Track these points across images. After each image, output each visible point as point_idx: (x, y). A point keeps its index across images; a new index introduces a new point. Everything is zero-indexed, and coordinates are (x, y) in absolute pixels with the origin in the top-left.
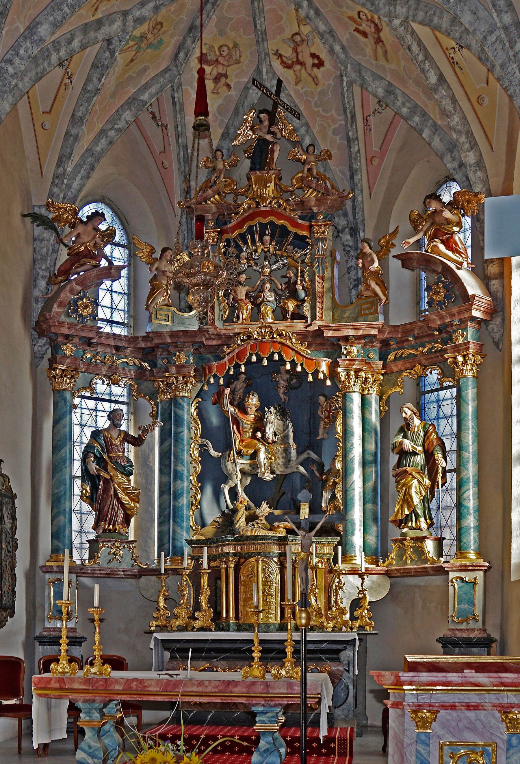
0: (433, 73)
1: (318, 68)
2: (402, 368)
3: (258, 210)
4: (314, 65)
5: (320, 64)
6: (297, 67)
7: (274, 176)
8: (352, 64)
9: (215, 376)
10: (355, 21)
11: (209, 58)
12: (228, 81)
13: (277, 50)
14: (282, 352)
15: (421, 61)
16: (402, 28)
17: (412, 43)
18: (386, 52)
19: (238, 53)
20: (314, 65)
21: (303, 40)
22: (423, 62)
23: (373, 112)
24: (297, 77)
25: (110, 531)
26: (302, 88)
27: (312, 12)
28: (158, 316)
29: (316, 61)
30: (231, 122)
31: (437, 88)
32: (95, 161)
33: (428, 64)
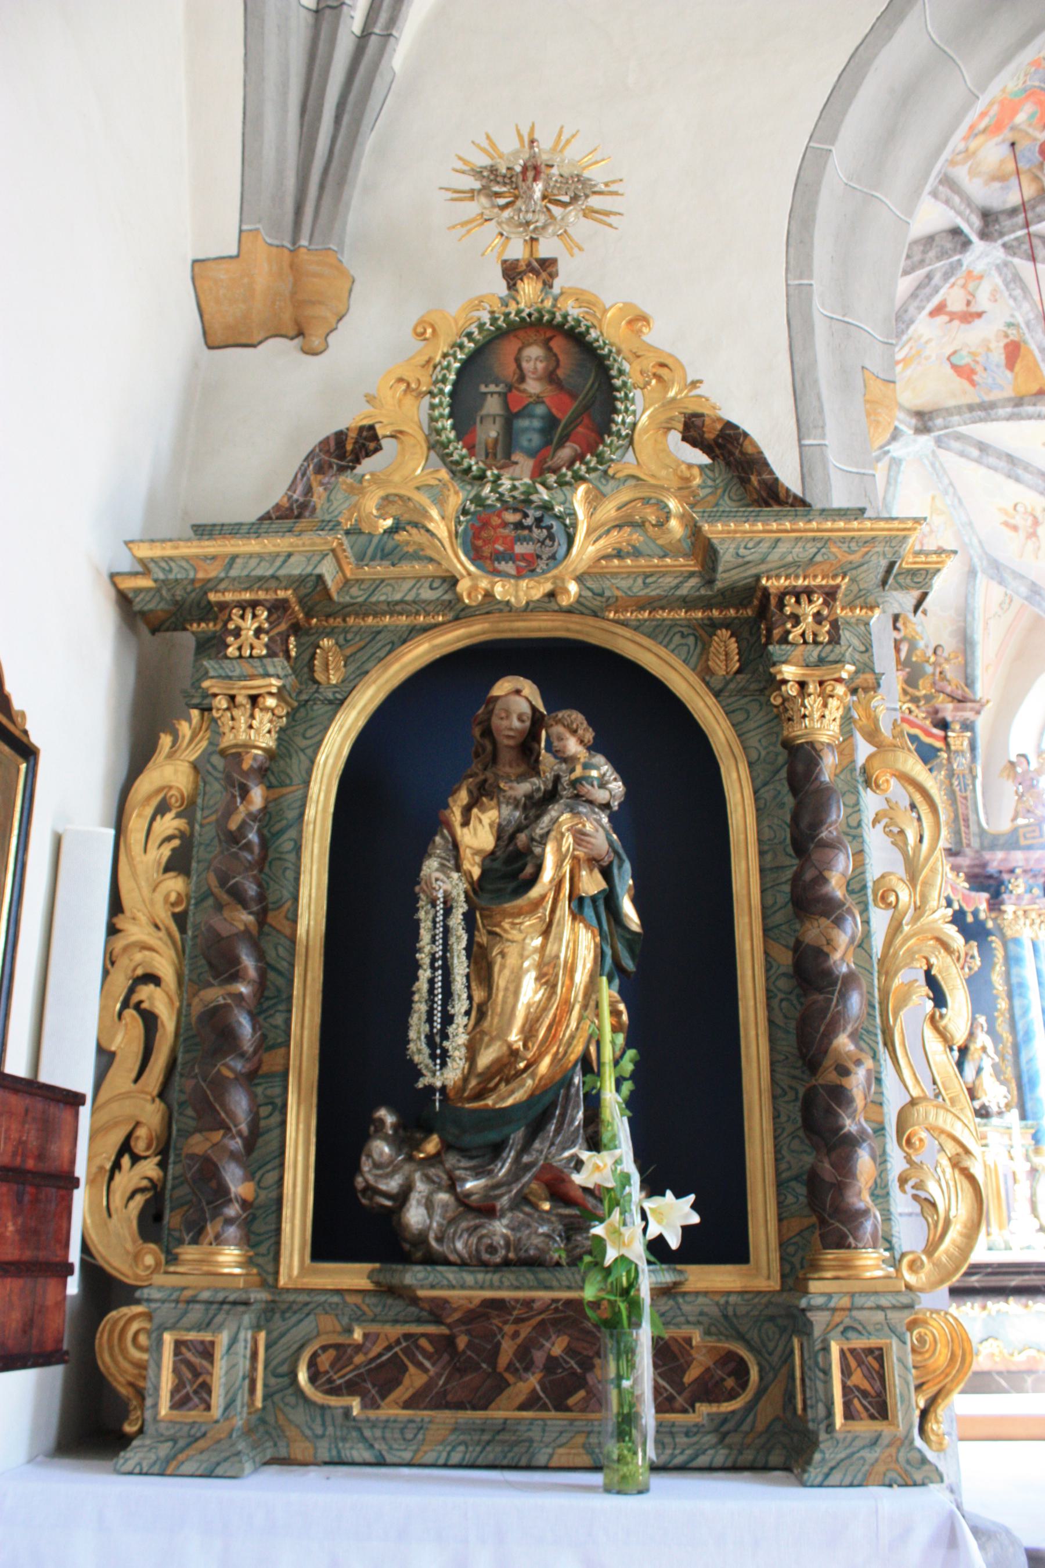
10: (1006, 513)
18: (1039, 548)
21: (931, 531)
27: (956, 501)
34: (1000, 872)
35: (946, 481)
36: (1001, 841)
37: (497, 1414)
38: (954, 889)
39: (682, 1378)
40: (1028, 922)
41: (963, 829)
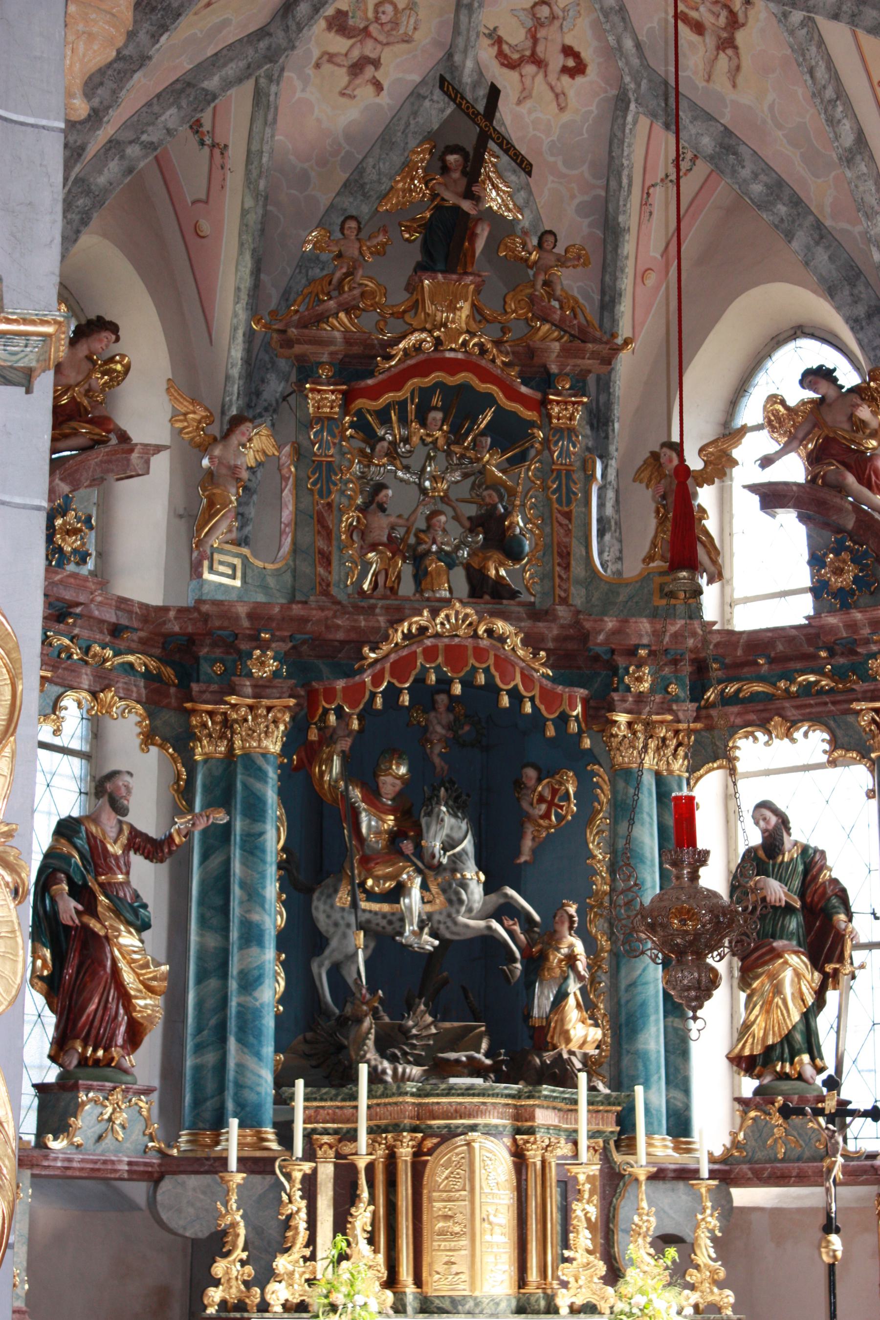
0: (848, 127)
1: (572, 76)
2: (738, 721)
3: (438, 355)
4: (565, 70)
5: (578, 69)
7: (472, 287)
8: (650, 81)
9: (339, 712)
11: (351, 22)
12: (379, 75)
13: (495, 29)
14: (493, 670)
15: (829, 101)
16: (804, 31)
17: (817, 63)
18: (738, 68)
19: (412, 21)
20: (565, 70)
21: (553, 17)
22: (832, 102)
23: (662, 180)
24: (524, 89)
25: (97, 1062)
26: (530, 112)
28: (216, 565)
29: (571, 63)
30: (371, 161)
31: (852, 158)
32: (94, 206)
33: (840, 109)
37: (339, 158)
38: (527, 679)
40: (652, 744)
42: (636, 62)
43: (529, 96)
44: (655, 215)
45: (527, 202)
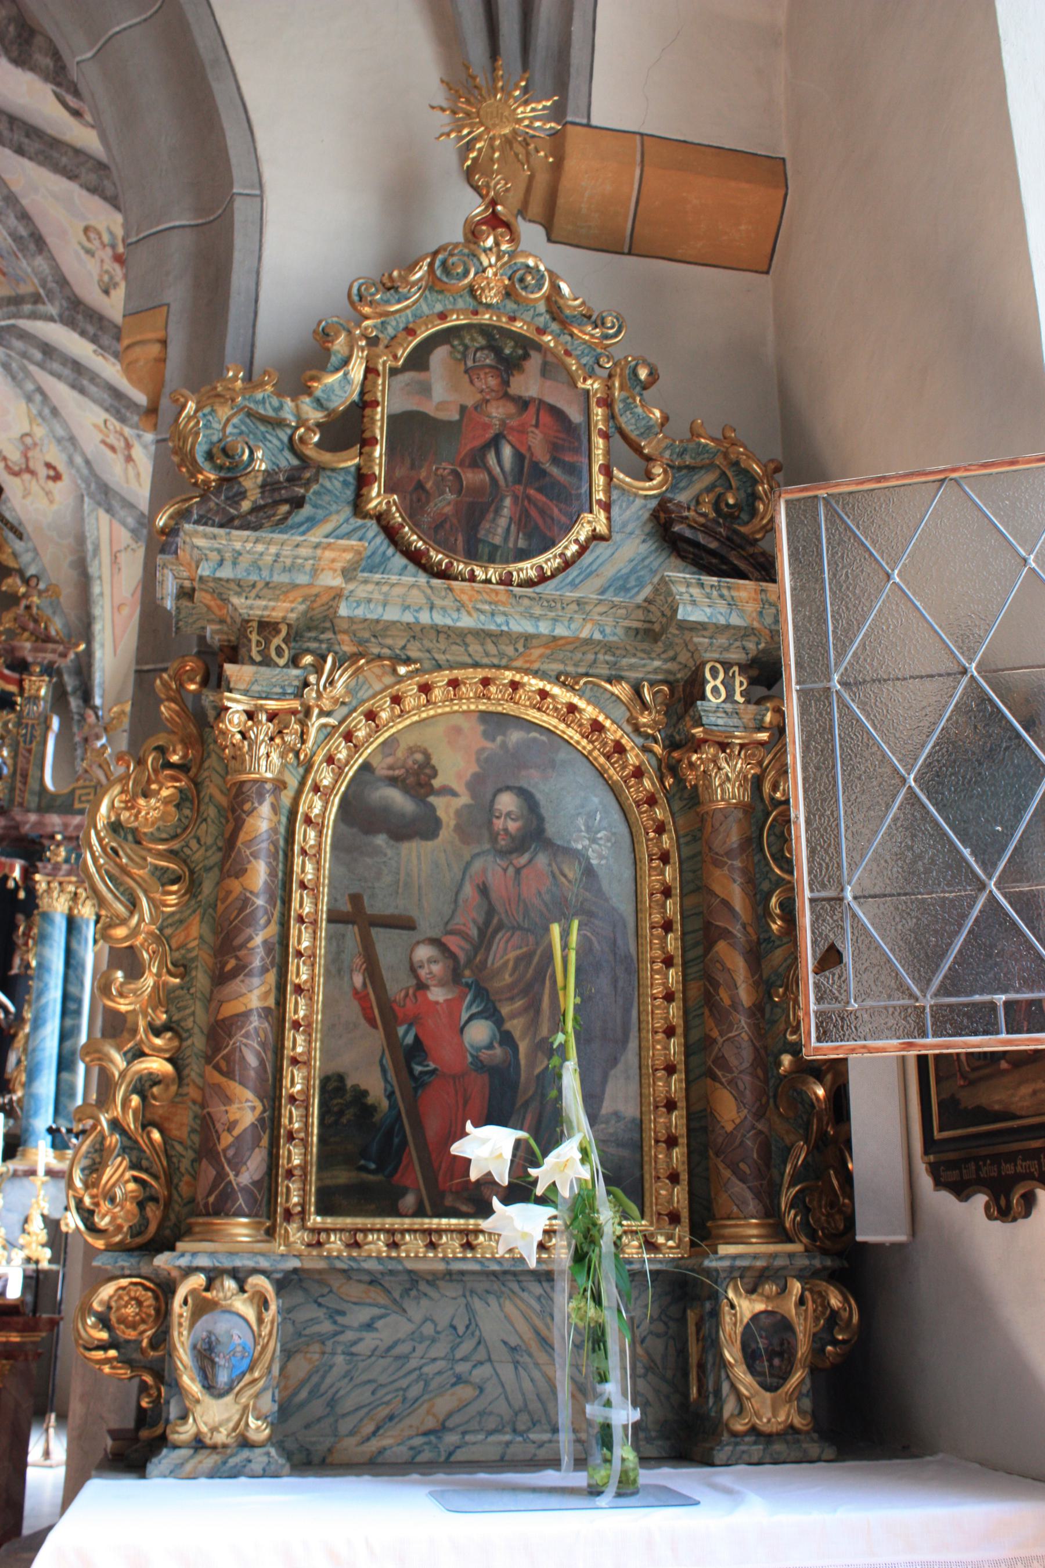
5: (57, 477)
6: (27, 477)
10: (101, 431)
20: (49, 477)
27: (46, 411)
29: (52, 473)
34: (41, 836)
35: (30, 386)
36: (58, 802)
39: (642, 1419)
41: (19, 785)
42: (85, 471)
43: (29, 494)
44: (123, 570)
45: (34, 560)
